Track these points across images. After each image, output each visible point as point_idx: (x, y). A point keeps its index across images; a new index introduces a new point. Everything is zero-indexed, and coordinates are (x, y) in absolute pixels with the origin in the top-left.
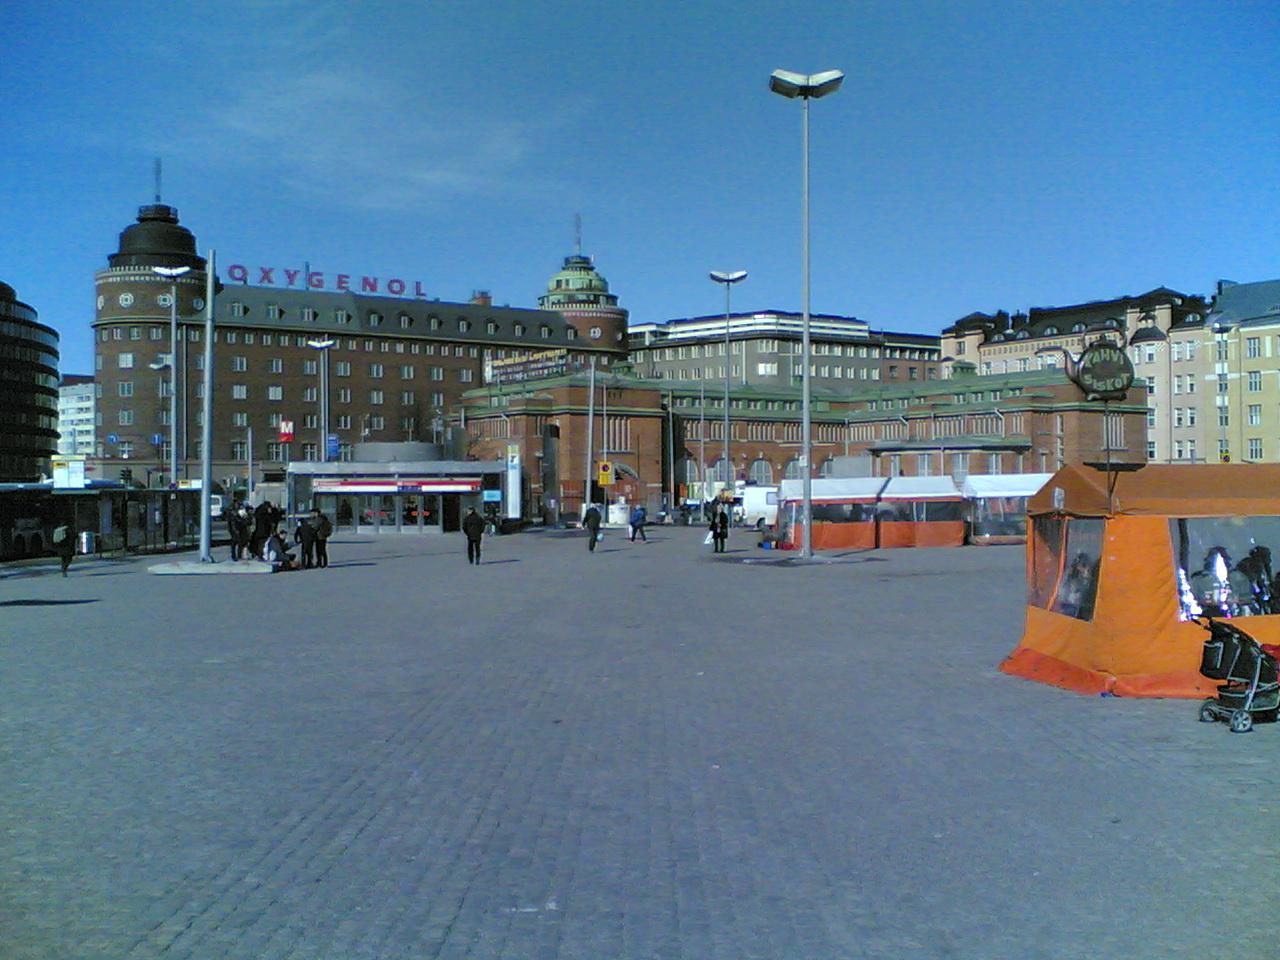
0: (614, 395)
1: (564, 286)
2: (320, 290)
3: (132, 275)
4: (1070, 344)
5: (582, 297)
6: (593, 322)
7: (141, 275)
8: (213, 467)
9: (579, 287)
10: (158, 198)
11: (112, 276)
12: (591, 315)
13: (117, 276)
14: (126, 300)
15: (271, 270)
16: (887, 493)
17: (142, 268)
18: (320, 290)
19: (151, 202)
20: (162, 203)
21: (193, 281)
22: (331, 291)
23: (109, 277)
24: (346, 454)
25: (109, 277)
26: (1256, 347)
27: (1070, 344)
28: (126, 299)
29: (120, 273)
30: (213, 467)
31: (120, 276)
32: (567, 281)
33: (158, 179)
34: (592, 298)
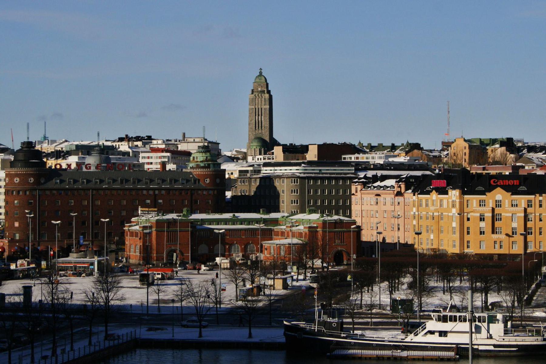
0: (173, 224)
1: (195, 160)
2: (89, 170)
3: (24, 171)
4: (259, 159)
5: (202, 165)
6: (206, 176)
7: (20, 171)
8: (333, 233)
9: (202, 160)
10: (28, 138)
11: (12, 171)
12: (19, 172)
13: (13, 171)
14: (17, 180)
15: (71, 164)
16: (529, 250)
17: (207, 169)
18: (89, 170)
19: (26, 140)
20: (30, 140)
21: (37, 172)
22: (94, 171)
23: (11, 171)
24: (482, 205)
25: (11, 171)
26: (260, 120)
27: (259, 159)
28: (17, 180)
29: (14, 170)
30: (333, 233)
31: (15, 171)
32: (197, 157)
33: (28, 131)
34: (206, 165)
